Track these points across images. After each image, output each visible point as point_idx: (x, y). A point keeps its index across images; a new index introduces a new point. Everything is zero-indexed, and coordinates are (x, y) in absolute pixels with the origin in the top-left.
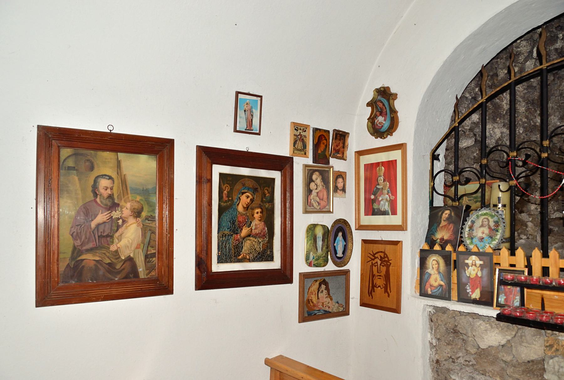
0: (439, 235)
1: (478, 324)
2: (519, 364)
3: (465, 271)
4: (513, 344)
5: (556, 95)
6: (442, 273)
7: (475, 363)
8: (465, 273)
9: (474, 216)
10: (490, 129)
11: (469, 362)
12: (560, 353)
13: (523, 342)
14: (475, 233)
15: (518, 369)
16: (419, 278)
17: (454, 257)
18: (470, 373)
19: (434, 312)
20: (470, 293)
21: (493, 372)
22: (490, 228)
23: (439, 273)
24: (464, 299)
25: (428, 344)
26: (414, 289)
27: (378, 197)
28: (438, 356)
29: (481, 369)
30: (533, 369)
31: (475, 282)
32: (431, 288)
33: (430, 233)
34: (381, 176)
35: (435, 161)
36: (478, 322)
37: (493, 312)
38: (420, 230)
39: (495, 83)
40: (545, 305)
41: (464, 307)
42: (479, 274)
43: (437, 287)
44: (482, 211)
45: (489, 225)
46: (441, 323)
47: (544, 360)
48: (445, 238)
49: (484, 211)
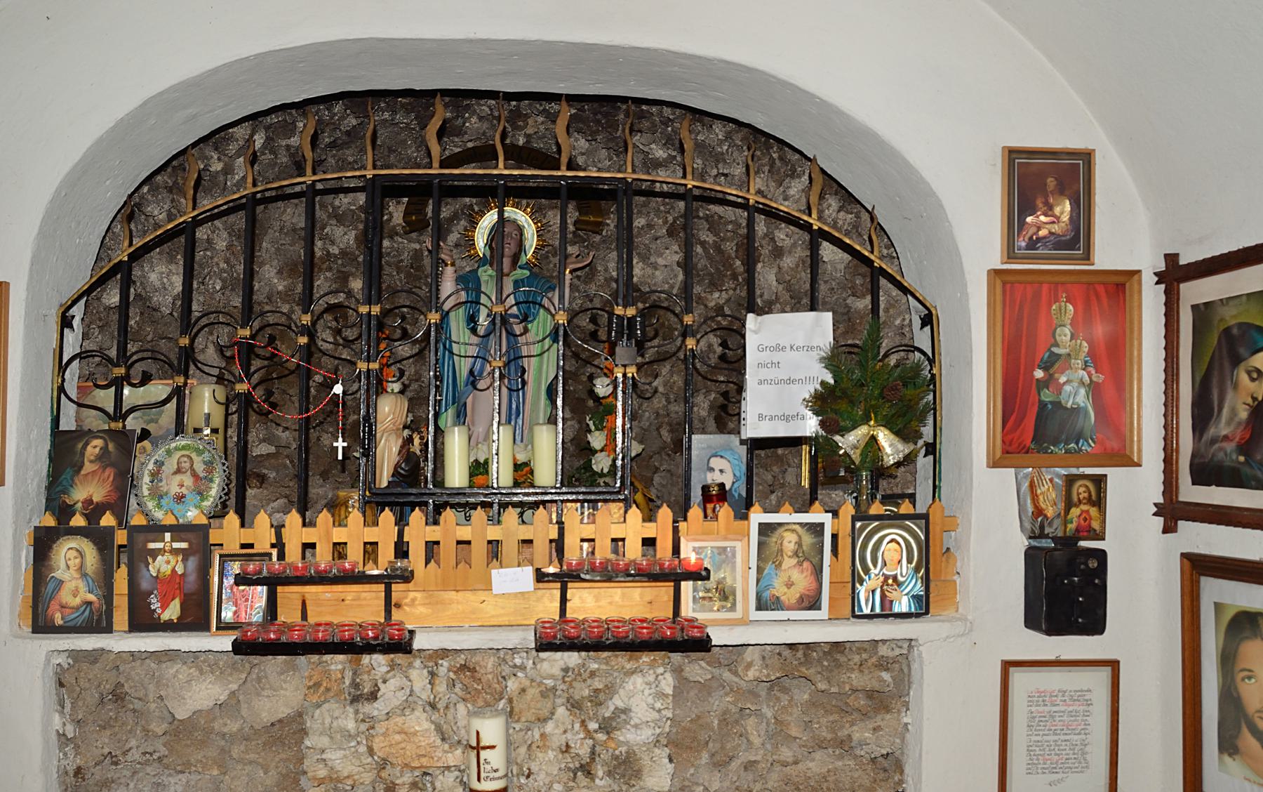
0: (79, 494)
1: (172, 671)
2: (256, 732)
3: (147, 565)
4: (241, 698)
5: (275, 228)
6: (92, 575)
7: (167, 753)
8: (148, 570)
9: (161, 452)
10: (163, 273)
11: (151, 754)
12: (332, 695)
13: (263, 689)
14: (164, 486)
15: (253, 743)
16: (31, 593)
17: (121, 537)
18: (154, 776)
19: (69, 664)
20: (159, 611)
21: (205, 761)
22: (195, 475)
23: (84, 575)
24: (142, 621)
25: (54, 737)
26: (18, 621)
27: (1056, 375)
28: (81, 759)
29: (180, 762)
30: (282, 735)
31: (170, 585)
32: (62, 613)
33: (58, 489)
34: (1064, 326)
35: (66, 331)
36: (172, 668)
37: (224, 643)
38: (32, 484)
39: (178, 184)
40: (308, 612)
41: (148, 641)
42: (180, 570)
43: (77, 608)
44: (178, 440)
45: (194, 470)
46: (87, 685)
47: (300, 715)
48: (96, 499)
49: (181, 442)
